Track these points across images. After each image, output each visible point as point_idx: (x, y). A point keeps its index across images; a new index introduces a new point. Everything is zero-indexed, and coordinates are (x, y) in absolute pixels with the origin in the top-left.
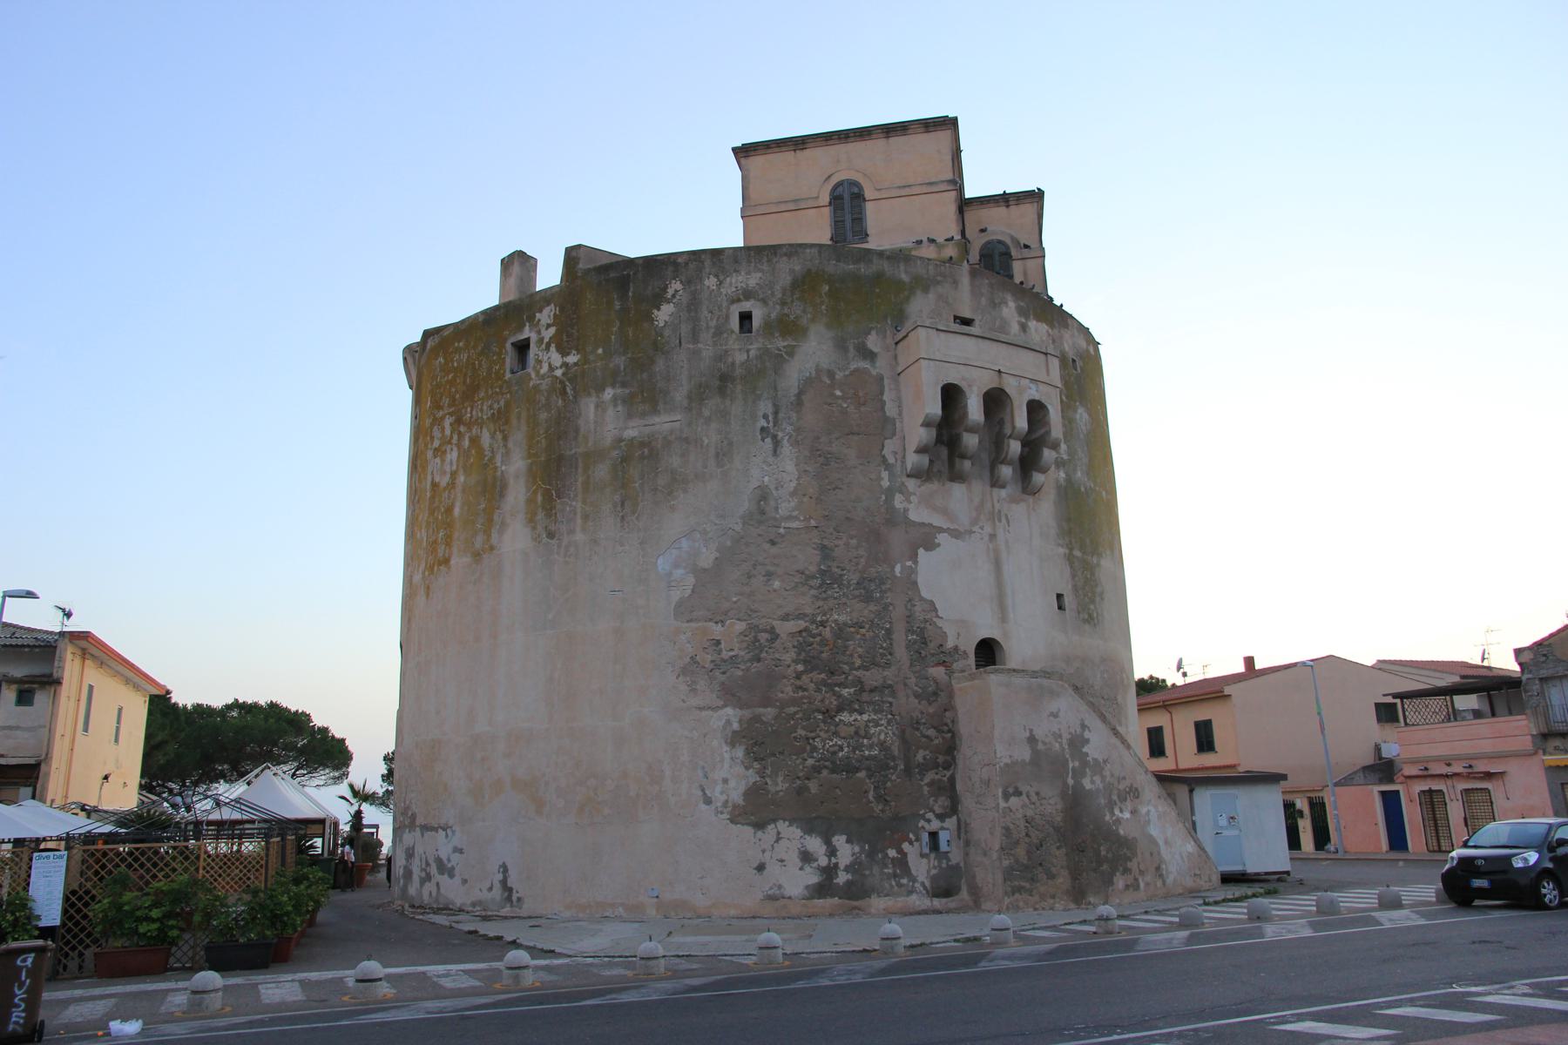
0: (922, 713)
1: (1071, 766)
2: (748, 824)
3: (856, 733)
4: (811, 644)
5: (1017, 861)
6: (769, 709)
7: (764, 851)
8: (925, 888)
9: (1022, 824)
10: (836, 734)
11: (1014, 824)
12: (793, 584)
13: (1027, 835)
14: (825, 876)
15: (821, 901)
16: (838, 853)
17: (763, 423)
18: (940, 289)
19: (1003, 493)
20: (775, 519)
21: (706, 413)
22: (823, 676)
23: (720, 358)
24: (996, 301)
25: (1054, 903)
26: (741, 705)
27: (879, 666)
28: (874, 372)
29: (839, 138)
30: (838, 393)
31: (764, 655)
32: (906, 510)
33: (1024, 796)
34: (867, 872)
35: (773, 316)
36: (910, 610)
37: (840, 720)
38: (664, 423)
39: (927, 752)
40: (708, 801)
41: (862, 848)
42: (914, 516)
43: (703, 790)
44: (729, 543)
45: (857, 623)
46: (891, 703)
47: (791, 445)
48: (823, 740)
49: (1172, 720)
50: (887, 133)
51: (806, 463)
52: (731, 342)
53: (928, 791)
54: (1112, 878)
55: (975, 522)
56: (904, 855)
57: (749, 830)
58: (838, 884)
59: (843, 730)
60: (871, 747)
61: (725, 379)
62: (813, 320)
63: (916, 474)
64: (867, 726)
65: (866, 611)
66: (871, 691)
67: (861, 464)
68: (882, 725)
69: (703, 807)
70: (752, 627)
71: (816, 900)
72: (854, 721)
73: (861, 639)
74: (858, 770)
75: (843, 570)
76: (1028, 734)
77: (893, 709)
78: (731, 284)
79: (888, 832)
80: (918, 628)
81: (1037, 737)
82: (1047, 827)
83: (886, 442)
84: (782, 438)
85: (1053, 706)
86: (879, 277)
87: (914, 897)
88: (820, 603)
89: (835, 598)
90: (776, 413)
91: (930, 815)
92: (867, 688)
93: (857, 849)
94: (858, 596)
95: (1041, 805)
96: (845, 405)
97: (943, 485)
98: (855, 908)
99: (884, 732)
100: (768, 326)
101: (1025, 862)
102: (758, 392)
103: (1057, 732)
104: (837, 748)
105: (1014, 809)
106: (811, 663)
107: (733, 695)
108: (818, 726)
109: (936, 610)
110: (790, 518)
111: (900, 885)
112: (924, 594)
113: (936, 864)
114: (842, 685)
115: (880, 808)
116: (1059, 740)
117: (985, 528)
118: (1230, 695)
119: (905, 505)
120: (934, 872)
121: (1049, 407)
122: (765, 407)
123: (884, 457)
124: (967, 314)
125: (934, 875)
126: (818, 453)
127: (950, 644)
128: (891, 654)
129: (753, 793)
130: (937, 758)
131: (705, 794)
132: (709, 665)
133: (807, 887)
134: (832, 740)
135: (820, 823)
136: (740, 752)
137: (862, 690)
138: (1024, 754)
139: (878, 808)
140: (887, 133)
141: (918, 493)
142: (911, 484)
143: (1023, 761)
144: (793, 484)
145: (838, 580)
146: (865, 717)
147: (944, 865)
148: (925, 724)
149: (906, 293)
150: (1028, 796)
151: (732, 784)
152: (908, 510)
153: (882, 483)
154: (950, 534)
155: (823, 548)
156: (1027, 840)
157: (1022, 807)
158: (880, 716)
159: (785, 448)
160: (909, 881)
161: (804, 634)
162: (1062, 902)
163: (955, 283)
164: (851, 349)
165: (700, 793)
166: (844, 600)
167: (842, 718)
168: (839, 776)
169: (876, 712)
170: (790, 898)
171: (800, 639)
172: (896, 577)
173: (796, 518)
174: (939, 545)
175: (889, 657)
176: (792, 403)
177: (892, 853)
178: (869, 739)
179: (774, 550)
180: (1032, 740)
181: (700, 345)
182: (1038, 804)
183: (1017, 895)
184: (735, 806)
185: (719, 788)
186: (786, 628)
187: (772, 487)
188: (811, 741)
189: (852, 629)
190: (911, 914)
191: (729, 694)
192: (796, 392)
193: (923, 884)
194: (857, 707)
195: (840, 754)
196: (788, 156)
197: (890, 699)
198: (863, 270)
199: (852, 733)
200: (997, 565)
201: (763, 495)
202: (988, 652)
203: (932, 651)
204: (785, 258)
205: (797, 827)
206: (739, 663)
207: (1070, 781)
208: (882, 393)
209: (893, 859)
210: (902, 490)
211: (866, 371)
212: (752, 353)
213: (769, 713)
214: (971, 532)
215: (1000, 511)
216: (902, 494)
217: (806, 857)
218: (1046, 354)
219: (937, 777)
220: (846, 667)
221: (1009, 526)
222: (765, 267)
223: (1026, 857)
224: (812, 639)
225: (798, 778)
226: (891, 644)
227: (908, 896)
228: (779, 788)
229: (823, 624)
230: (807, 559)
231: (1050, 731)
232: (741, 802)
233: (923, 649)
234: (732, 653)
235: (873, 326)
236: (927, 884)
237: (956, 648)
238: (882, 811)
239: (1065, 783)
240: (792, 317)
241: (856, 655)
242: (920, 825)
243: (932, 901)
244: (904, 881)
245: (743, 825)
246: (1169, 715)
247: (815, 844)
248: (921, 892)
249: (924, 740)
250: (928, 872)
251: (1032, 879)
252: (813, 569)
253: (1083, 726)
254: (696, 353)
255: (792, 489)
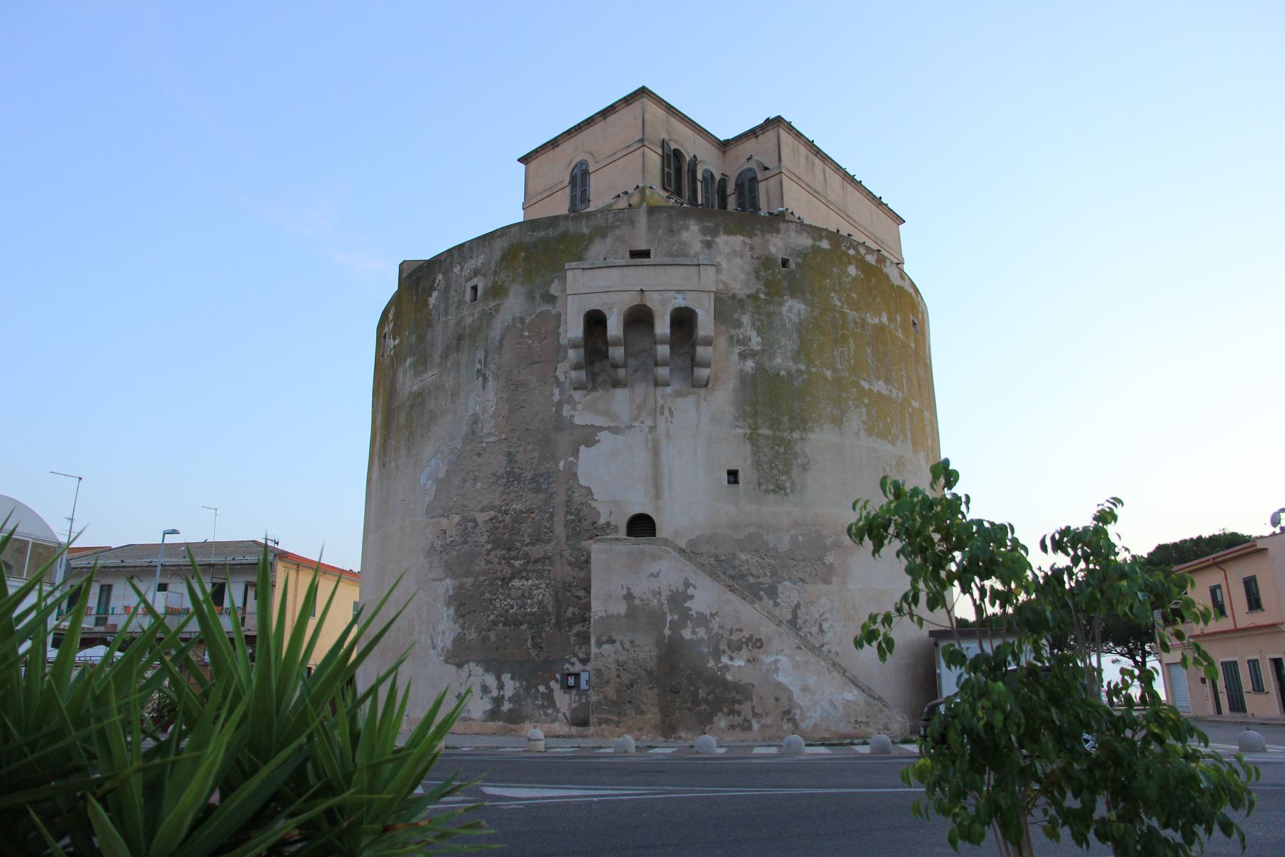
0: (574, 578)
1: (669, 618)
2: (454, 664)
3: (523, 595)
4: (498, 528)
5: (606, 698)
6: (469, 579)
7: (461, 684)
8: (566, 718)
9: (613, 666)
10: (509, 595)
11: (605, 667)
12: (489, 484)
13: (618, 676)
14: (495, 705)
15: (492, 723)
16: (505, 687)
17: (478, 366)
18: (617, 232)
19: (668, 390)
20: (482, 437)
21: (449, 365)
22: (503, 552)
23: (458, 323)
24: (675, 229)
25: (641, 735)
26: (455, 577)
27: (543, 542)
28: (554, 312)
29: (576, 130)
30: (527, 334)
31: (469, 539)
32: (572, 417)
33: (618, 644)
34: (524, 703)
35: (489, 284)
36: (570, 496)
37: (512, 585)
38: (429, 377)
39: (576, 609)
40: (434, 648)
41: (521, 685)
42: (578, 421)
43: (432, 639)
44: (454, 459)
45: (529, 509)
46: (549, 571)
47: (494, 380)
48: (501, 601)
49: (1226, 578)
50: (604, 115)
51: (503, 391)
52: (465, 311)
53: (574, 640)
54: (712, 718)
55: (635, 418)
56: (551, 691)
57: (454, 668)
58: (503, 711)
59: (514, 593)
60: (532, 606)
61: (460, 338)
62: (512, 282)
63: (579, 387)
64: (531, 589)
65: (536, 500)
66: (536, 562)
67: (539, 386)
68: (542, 588)
69: (432, 651)
70: (465, 519)
71: (489, 723)
72: (522, 585)
73: (531, 522)
74: (521, 624)
75: (522, 470)
76: (625, 592)
77: (551, 575)
78: (468, 267)
79: (540, 672)
80: (576, 509)
81: (634, 594)
82: (639, 669)
83: (559, 365)
84: (489, 376)
85: (654, 568)
86: (564, 236)
87: (556, 725)
88: (506, 496)
89: (515, 492)
90: (486, 358)
91: (574, 660)
92: (532, 560)
93: (518, 685)
94: (531, 489)
95: (635, 651)
96: (530, 342)
97: (607, 392)
98: (512, 730)
99: (543, 594)
100: (486, 293)
101: (614, 699)
102: (477, 344)
103: (657, 590)
104: (509, 606)
105: (606, 655)
106: (496, 543)
107: (451, 570)
108: (498, 590)
109: (591, 494)
110: (490, 434)
111: (546, 714)
112: (582, 482)
113: (577, 699)
114: (516, 558)
115: (536, 653)
116: (658, 597)
117: (645, 423)
118: (1266, 549)
119: (572, 412)
120: (574, 705)
121: (697, 311)
122: (480, 354)
123: (556, 377)
124: (642, 246)
125: (574, 708)
126: (512, 382)
127: (602, 521)
128: (552, 532)
129: (458, 640)
130: (585, 614)
131: (433, 642)
132: (439, 549)
133: (484, 712)
134: (506, 601)
135: (495, 666)
136: (452, 611)
137: (529, 562)
138: (622, 608)
139: (534, 653)
140: (604, 115)
141: (583, 402)
142: (578, 395)
143: (619, 614)
144: (493, 409)
145: (518, 478)
146: (530, 582)
147: (584, 701)
148: (576, 586)
149: (586, 243)
150: (622, 645)
151: (447, 634)
152: (574, 416)
153: (554, 398)
154: (610, 431)
155: (509, 454)
156: (617, 680)
157: (615, 653)
158: (540, 581)
159: (490, 383)
160: (554, 712)
161: (494, 521)
162: (649, 735)
163: (633, 223)
164: (538, 297)
165: (430, 641)
166: (521, 493)
167: (514, 584)
168: (508, 629)
169: (537, 578)
170: (474, 720)
171: (491, 525)
172: (560, 471)
173: (493, 434)
174: (599, 441)
175: (551, 534)
176: (496, 348)
177: (542, 689)
178: (532, 599)
179: (479, 460)
180: (629, 597)
181: (448, 317)
182: (631, 650)
183: (604, 726)
184: (448, 651)
185: (440, 638)
186: (482, 517)
187: (480, 413)
188: (494, 602)
189: (525, 515)
190: (553, 737)
191: (450, 570)
192: (499, 339)
193: (564, 715)
194: (524, 574)
195: (511, 611)
196: (550, 154)
197: (549, 568)
198: (551, 233)
199: (520, 595)
200: (655, 452)
201: (475, 420)
202: (642, 525)
203: (586, 528)
204: (498, 240)
205: (481, 667)
206: (455, 546)
207: (667, 632)
208: (559, 328)
209: (542, 694)
210: (570, 401)
211: (548, 312)
212: (476, 316)
213: (469, 581)
214: (632, 427)
215: (663, 406)
216: (569, 404)
217: (485, 689)
218: (699, 265)
219: (583, 629)
220: (519, 544)
221: (672, 417)
222: (487, 250)
223: (615, 695)
224: (498, 525)
225: (483, 630)
226: (552, 524)
227: (552, 723)
228: (471, 637)
229: (506, 513)
230: (498, 463)
231: (648, 589)
232: (451, 648)
233: (578, 526)
234: (452, 539)
235: (556, 275)
236: (568, 715)
237: (608, 524)
238: (537, 655)
239: (661, 634)
240: (500, 282)
241: (526, 535)
242: (565, 667)
243: (570, 728)
244: (550, 711)
245: (451, 664)
246: (1223, 573)
247: (491, 680)
248: (562, 721)
249: (573, 599)
250: (570, 705)
251: (620, 713)
252: (502, 471)
253: (687, 584)
254: (447, 322)
255: (492, 413)
